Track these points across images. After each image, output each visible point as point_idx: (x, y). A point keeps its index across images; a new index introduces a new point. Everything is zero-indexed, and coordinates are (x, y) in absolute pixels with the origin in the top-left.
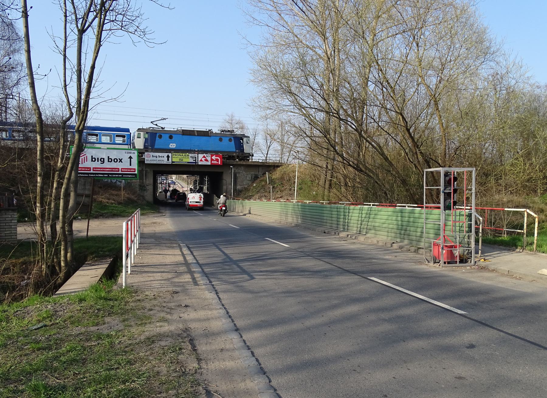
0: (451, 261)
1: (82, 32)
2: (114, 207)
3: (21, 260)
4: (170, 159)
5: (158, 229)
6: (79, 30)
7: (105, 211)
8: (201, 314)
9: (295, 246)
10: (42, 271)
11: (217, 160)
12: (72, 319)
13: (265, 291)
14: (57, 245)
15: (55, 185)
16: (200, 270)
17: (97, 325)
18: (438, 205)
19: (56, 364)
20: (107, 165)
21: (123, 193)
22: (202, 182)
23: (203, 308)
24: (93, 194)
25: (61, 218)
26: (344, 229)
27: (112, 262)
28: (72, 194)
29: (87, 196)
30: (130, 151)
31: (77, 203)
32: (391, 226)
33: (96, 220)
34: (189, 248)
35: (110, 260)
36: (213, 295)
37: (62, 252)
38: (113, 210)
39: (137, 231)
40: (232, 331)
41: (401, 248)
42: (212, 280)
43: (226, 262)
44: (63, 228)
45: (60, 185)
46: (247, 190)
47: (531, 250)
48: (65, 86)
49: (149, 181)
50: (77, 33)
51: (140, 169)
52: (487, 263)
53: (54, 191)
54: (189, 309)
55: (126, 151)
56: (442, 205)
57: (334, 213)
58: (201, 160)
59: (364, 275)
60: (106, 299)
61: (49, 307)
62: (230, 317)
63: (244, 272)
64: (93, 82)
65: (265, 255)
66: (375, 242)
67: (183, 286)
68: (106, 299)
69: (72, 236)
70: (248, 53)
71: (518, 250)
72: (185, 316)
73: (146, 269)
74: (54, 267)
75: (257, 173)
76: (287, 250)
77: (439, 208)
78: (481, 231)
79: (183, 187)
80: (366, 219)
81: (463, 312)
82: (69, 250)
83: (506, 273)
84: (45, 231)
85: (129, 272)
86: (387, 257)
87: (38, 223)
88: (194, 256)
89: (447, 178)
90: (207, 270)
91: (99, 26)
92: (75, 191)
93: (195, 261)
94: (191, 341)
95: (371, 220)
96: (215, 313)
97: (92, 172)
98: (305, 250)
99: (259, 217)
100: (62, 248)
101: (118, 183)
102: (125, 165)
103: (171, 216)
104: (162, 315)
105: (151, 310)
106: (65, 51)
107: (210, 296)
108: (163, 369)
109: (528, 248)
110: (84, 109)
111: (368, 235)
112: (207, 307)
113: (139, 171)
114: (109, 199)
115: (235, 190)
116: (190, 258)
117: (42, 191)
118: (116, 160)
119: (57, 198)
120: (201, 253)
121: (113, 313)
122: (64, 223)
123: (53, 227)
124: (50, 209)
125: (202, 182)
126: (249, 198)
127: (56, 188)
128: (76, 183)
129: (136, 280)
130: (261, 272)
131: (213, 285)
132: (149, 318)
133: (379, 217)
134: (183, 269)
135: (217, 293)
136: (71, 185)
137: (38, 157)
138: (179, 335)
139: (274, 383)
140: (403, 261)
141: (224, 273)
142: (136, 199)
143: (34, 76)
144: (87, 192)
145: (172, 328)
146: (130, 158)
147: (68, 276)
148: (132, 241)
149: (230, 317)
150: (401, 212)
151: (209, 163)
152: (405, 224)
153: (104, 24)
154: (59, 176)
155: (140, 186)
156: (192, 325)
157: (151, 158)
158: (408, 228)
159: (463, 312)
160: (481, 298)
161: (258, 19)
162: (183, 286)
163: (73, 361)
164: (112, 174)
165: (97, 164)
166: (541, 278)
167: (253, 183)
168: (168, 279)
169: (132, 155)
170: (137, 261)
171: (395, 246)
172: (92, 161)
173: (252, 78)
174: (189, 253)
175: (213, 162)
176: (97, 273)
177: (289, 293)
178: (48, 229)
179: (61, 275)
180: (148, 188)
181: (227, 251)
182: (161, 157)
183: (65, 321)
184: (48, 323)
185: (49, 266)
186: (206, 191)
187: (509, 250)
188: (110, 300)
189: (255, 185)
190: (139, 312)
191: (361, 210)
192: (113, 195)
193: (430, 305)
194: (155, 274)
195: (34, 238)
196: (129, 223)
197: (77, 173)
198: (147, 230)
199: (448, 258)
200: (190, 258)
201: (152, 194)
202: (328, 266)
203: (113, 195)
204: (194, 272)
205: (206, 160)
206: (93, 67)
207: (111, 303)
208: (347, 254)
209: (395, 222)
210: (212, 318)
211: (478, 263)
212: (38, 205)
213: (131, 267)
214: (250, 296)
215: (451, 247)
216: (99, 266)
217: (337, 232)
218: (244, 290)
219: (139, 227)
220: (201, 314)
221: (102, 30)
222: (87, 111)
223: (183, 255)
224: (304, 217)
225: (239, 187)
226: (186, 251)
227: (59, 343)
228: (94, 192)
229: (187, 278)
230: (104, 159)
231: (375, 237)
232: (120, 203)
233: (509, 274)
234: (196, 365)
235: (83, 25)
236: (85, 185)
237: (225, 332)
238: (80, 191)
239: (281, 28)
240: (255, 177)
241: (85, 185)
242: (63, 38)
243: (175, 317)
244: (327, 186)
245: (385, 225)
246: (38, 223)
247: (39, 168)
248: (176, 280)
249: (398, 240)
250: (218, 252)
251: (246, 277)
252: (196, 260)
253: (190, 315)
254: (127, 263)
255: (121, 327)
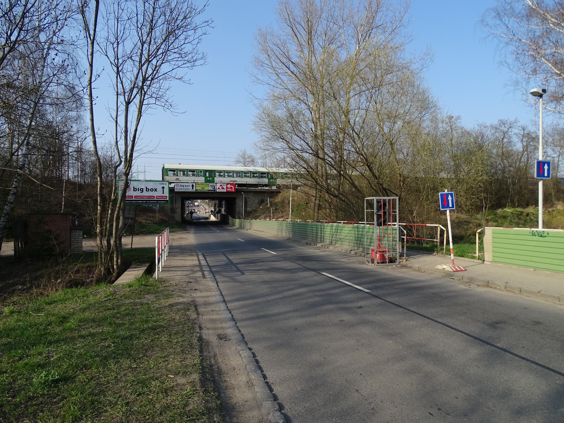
0: (383, 261)
1: (128, 103)
2: (151, 226)
3: (87, 264)
4: (194, 188)
5: (183, 243)
6: (126, 103)
7: (144, 230)
8: (205, 294)
9: (280, 253)
10: (101, 272)
11: (231, 188)
12: (126, 296)
13: (249, 281)
14: (111, 254)
15: (110, 212)
16: (209, 269)
17: (140, 299)
18: (373, 223)
19: (118, 315)
20: (145, 194)
21: (157, 215)
22: (220, 206)
23: (206, 291)
24: (135, 216)
25: (114, 234)
26: (321, 241)
27: (149, 265)
28: (121, 218)
29: (132, 219)
30: (163, 183)
31: (125, 224)
32: (351, 238)
33: (137, 236)
34: (204, 256)
35: (147, 265)
36: (215, 284)
37: (115, 259)
38: (150, 228)
39: (167, 243)
40: (221, 302)
41: (356, 254)
42: (216, 275)
43: (228, 264)
44: (115, 241)
45: (113, 211)
46: (255, 211)
47: (442, 254)
48: (117, 142)
49: (178, 205)
50: (125, 105)
51: (171, 196)
52: (408, 262)
53: (109, 216)
54: (197, 291)
55: (160, 182)
56: (375, 222)
57: (314, 229)
58: (219, 188)
59: (319, 272)
60: (145, 285)
61: (111, 289)
62: (222, 295)
63: (238, 270)
64: (136, 139)
65: (257, 260)
66: (340, 250)
67: (196, 279)
68: (145, 285)
69: (121, 248)
70: (254, 105)
71: (434, 254)
72: (194, 295)
73: (172, 269)
74: (109, 269)
75: (263, 198)
76: (275, 256)
77: (373, 224)
78: (405, 241)
79: (205, 209)
80: (335, 234)
81: (368, 291)
82: (120, 258)
83: (417, 269)
84: (103, 244)
85: (160, 271)
86: (343, 260)
87: (98, 239)
88: (206, 261)
89: (380, 204)
90: (213, 269)
91: (140, 102)
92: (123, 216)
93: (206, 264)
94: (196, 307)
95: (338, 234)
96: (213, 293)
97: (134, 199)
98: (288, 256)
99: (262, 233)
100: (115, 255)
101: (154, 207)
102: (159, 193)
103: (195, 233)
104: (180, 294)
105: (173, 291)
106: (117, 118)
107: (212, 284)
108: (178, 318)
109: (441, 252)
110: (130, 159)
111: (337, 245)
112: (210, 290)
113: (170, 197)
114: (147, 220)
115: (246, 211)
116: (203, 262)
117: (101, 216)
118: (152, 190)
119: (111, 220)
120: (212, 259)
121: (149, 293)
122: (116, 238)
123: (109, 242)
124: (106, 228)
125: (220, 206)
126: (256, 218)
127: (111, 214)
128: (124, 210)
129: (165, 275)
130: (250, 270)
131: (215, 279)
132: (172, 295)
133: (343, 231)
134: (198, 269)
135: (217, 283)
136: (121, 211)
137: (98, 192)
138: (188, 303)
139: (238, 325)
140: (353, 263)
141: (224, 271)
142: (167, 219)
143: (96, 136)
144: (131, 216)
145: (185, 300)
146: (163, 188)
147: (119, 275)
148: (162, 250)
149: (222, 295)
150: (357, 227)
151: (225, 191)
152: (360, 236)
153: (144, 100)
154: (112, 205)
155: (171, 209)
156: (197, 299)
157: (180, 187)
158: (362, 239)
159: (368, 291)
160: (388, 283)
161: (261, 79)
162: (196, 279)
163: (127, 314)
164: (149, 201)
165: (138, 193)
166: (436, 271)
167: (260, 205)
168: (186, 275)
169: (164, 186)
170: (166, 264)
171: (353, 252)
172: (134, 190)
173: (254, 128)
174: (203, 258)
175: (228, 190)
176: (139, 273)
177: (265, 282)
178: (105, 243)
179: (114, 274)
180: (177, 210)
181: (230, 258)
182: (188, 186)
183: (121, 297)
184: (111, 297)
185: (106, 269)
186: (224, 213)
187: (429, 254)
188: (148, 286)
189: (261, 207)
190: (166, 293)
191: (332, 226)
192: (150, 217)
193: (351, 287)
194: (177, 272)
195: (96, 249)
196: (160, 237)
197: (124, 203)
198: (175, 244)
199: (381, 259)
200: (203, 262)
201: (180, 215)
202: (299, 266)
203: (150, 217)
204: (205, 271)
205: (223, 188)
206: (136, 130)
207: (149, 288)
208: (316, 258)
209: (354, 235)
210: (211, 296)
211: (401, 263)
212: (98, 226)
213: (162, 268)
214: (239, 284)
215: (383, 252)
216: (140, 269)
217: (315, 242)
218: (235, 281)
219: (168, 241)
220: (205, 294)
221: (142, 105)
222: (132, 160)
223: (199, 260)
224: (294, 232)
225: (249, 209)
226: (201, 257)
227: (119, 307)
228: (136, 215)
229: (199, 274)
230: (143, 189)
231: (341, 246)
232: (155, 223)
233: (419, 270)
234: (196, 316)
235: (129, 99)
236: (129, 211)
237: (217, 303)
238: (126, 216)
239: (279, 86)
240: (261, 201)
241: (129, 211)
242: (116, 109)
243: (188, 295)
244: (316, 208)
245: (347, 238)
246: (98, 239)
247: (99, 200)
248: (192, 275)
249: (356, 248)
250: (225, 258)
251: (239, 273)
252: (208, 263)
253: (198, 294)
254: (159, 267)
255: (154, 299)
